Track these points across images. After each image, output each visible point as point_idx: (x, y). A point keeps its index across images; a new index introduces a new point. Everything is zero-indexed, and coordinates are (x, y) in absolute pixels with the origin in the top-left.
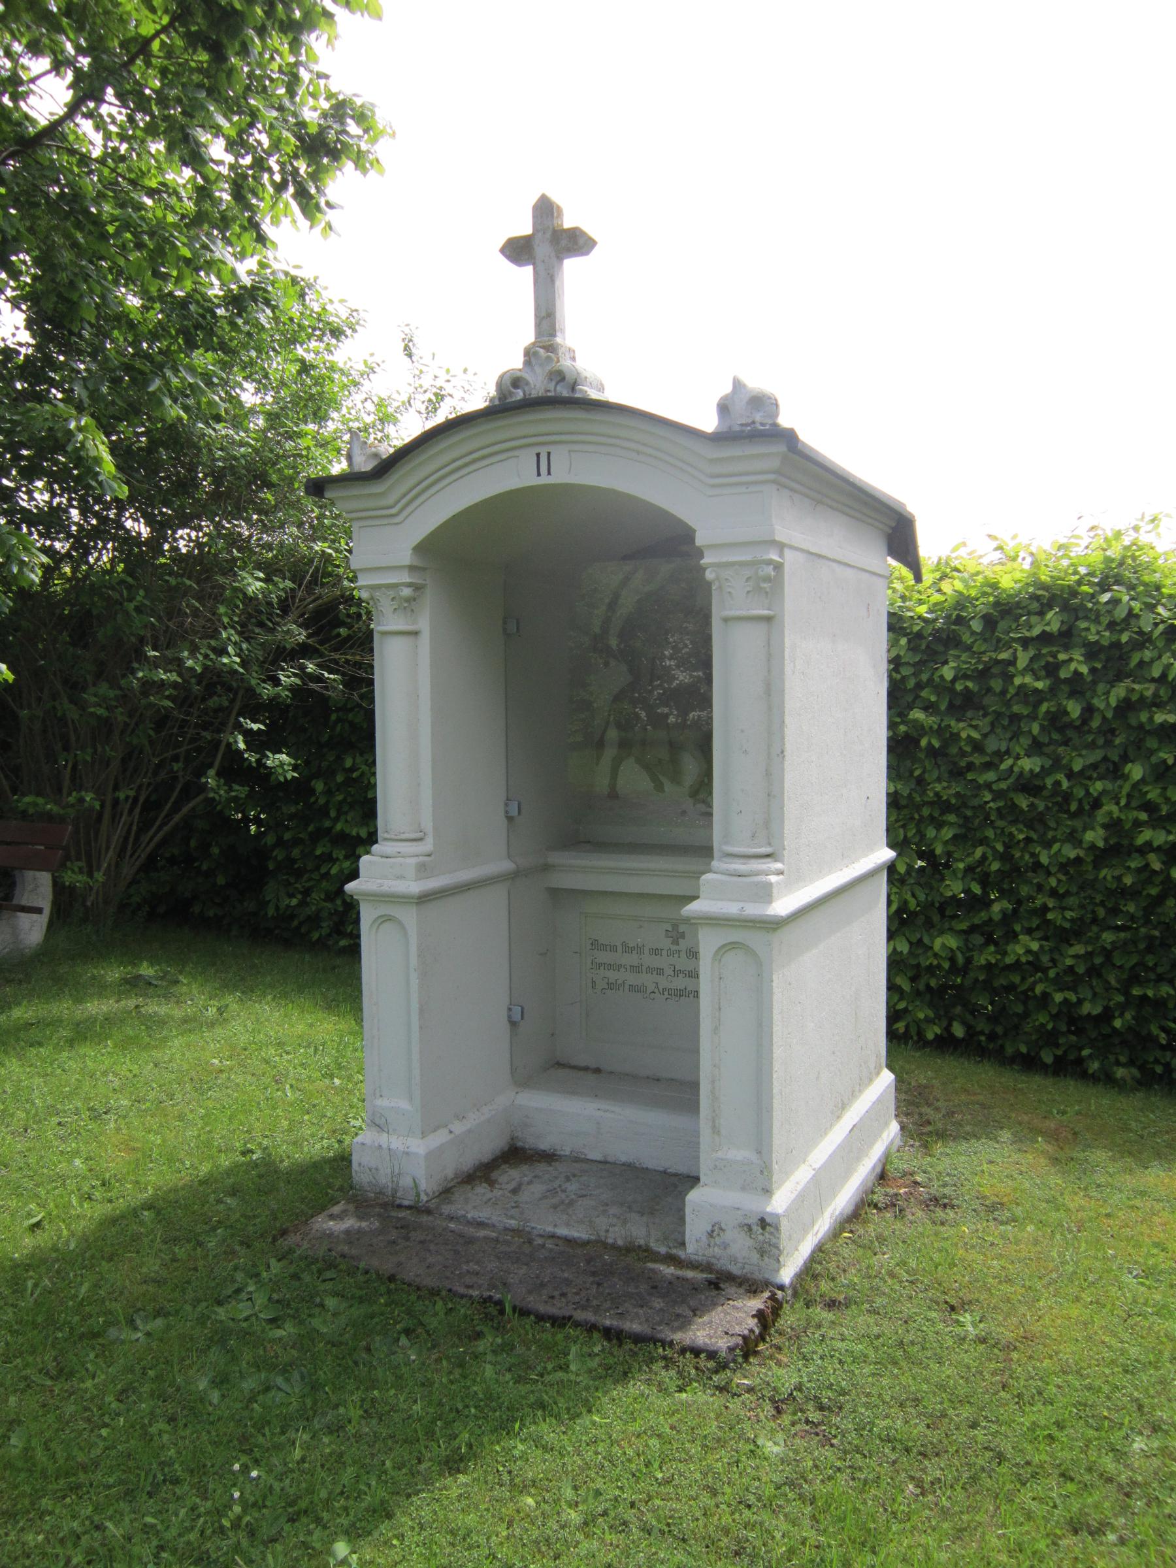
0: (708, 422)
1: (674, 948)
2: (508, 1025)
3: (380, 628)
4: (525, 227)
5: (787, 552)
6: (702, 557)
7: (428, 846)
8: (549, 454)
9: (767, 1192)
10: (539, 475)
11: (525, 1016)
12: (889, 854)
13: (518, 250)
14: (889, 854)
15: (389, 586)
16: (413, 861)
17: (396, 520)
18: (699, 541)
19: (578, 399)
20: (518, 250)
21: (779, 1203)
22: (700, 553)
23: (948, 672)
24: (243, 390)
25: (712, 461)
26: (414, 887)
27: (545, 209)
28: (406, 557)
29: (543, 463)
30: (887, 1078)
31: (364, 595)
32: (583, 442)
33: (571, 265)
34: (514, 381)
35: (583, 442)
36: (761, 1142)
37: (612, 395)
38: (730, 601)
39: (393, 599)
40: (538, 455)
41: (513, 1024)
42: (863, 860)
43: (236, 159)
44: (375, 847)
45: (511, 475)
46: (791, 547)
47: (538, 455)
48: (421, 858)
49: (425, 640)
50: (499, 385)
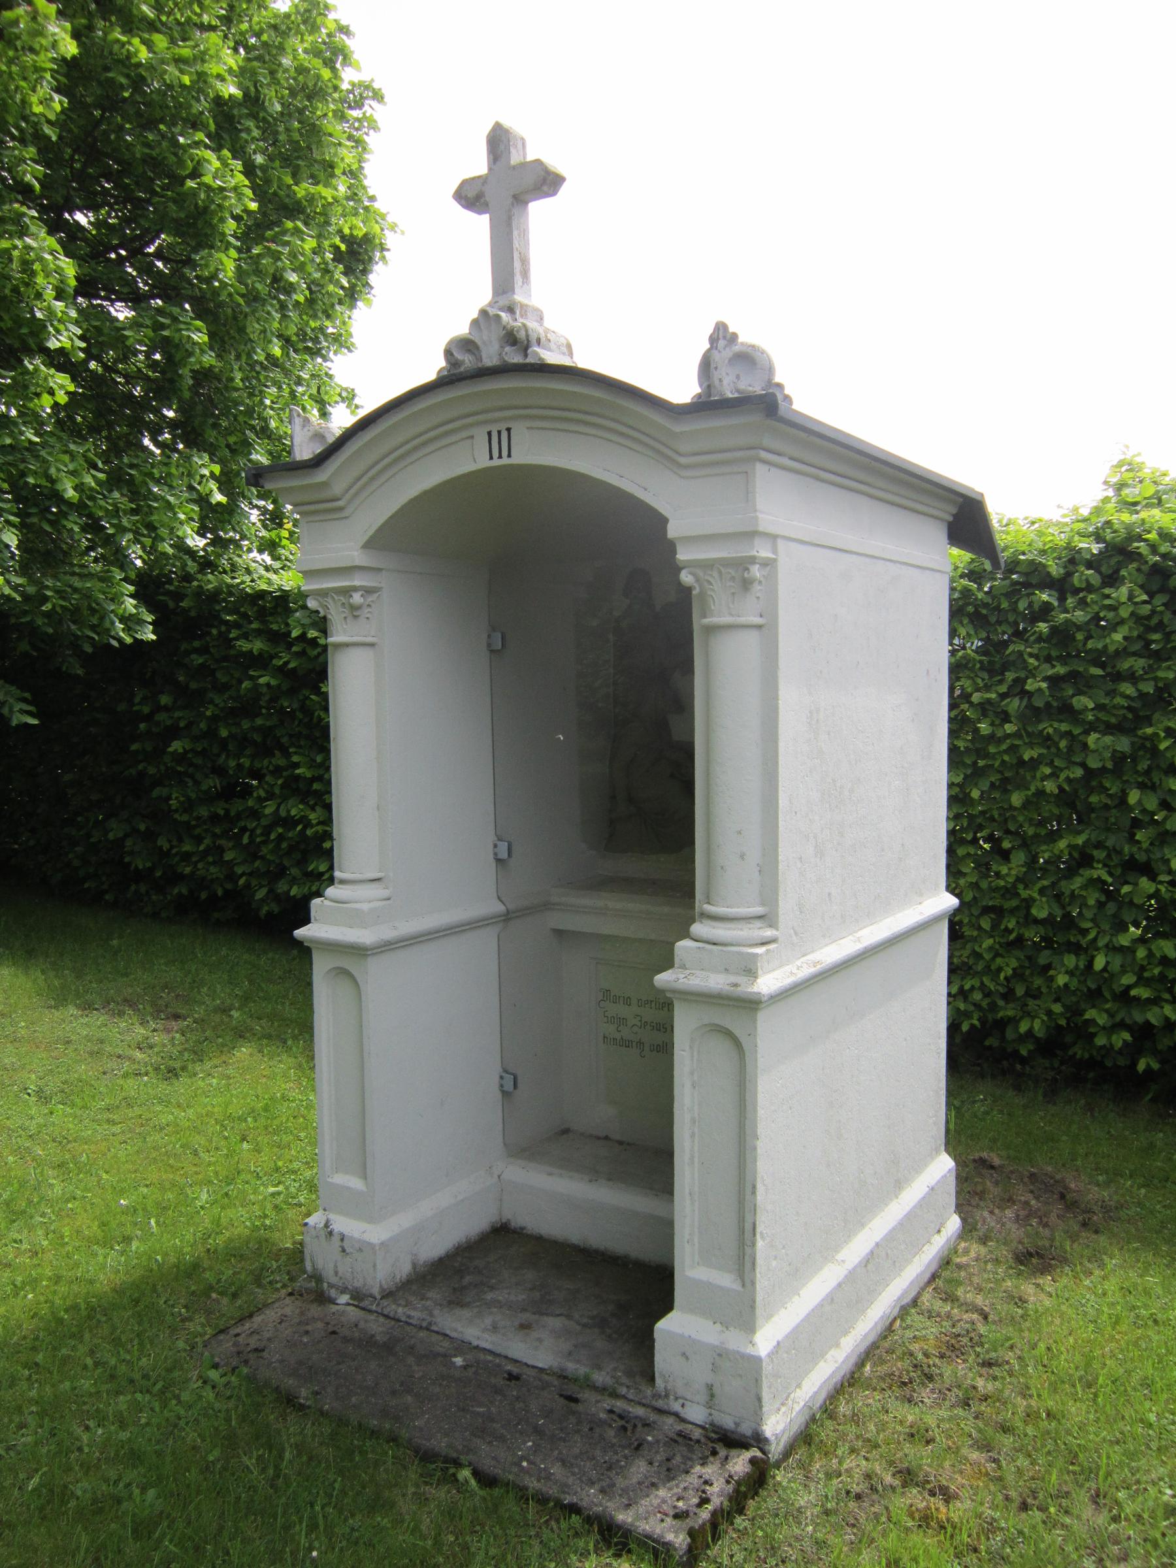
0: (679, 386)
2: (499, 1095)
4: (480, 166)
5: (781, 544)
9: (750, 1327)
10: (491, 458)
11: (519, 1085)
12: (952, 902)
13: (471, 196)
14: (952, 902)
18: (672, 532)
19: (532, 365)
20: (471, 196)
21: (764, 1341)
23: (262, 681)
27: (499, 141)
29: (500, 440)
30: (945, 1164)
32: (622, 434)
33: (538, 210)
34: (466, 344)
35: (622, 434)
36: (742, 1261)
37: (583, 360)
38: (718, 608)
40: (489, 434)
41: (505, 1094)
44: (330, 891)
45: (470, 458)
46: (784, 538)
47: (489, 434)
50: (448, 353)
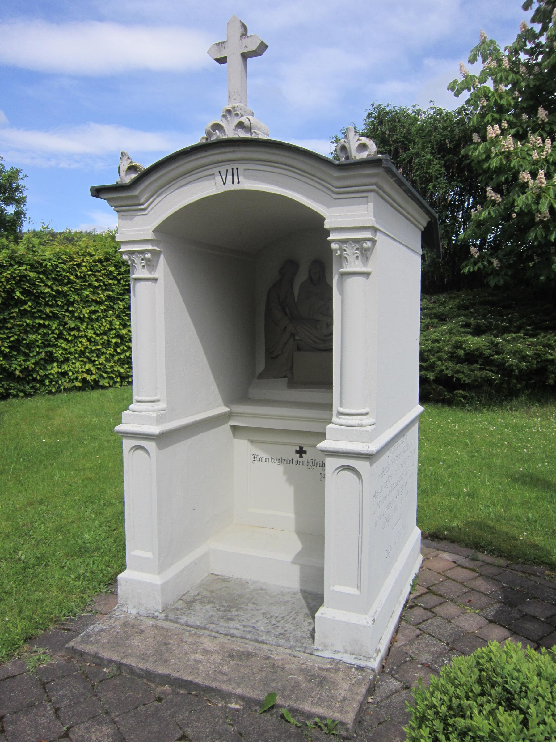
1: (300, 459)
3: (133, 276)
6: (329, 236)
7: (162, 405)
8: (237, 169)
10: (233, 183)
15: (142, 252)
16: (154, 415)
17: (146, 212)
18: (326, 226)
22: (327, 232)
24: (204, 643)
25: (338, 179)
26: (155, 430)
28: (150, 235)
31: (125, 257)
39: (142, 260)
42: (334, 280)
43: (145, 257)
47: (233, 169)
48: (158, 413)
49: (161, 281)
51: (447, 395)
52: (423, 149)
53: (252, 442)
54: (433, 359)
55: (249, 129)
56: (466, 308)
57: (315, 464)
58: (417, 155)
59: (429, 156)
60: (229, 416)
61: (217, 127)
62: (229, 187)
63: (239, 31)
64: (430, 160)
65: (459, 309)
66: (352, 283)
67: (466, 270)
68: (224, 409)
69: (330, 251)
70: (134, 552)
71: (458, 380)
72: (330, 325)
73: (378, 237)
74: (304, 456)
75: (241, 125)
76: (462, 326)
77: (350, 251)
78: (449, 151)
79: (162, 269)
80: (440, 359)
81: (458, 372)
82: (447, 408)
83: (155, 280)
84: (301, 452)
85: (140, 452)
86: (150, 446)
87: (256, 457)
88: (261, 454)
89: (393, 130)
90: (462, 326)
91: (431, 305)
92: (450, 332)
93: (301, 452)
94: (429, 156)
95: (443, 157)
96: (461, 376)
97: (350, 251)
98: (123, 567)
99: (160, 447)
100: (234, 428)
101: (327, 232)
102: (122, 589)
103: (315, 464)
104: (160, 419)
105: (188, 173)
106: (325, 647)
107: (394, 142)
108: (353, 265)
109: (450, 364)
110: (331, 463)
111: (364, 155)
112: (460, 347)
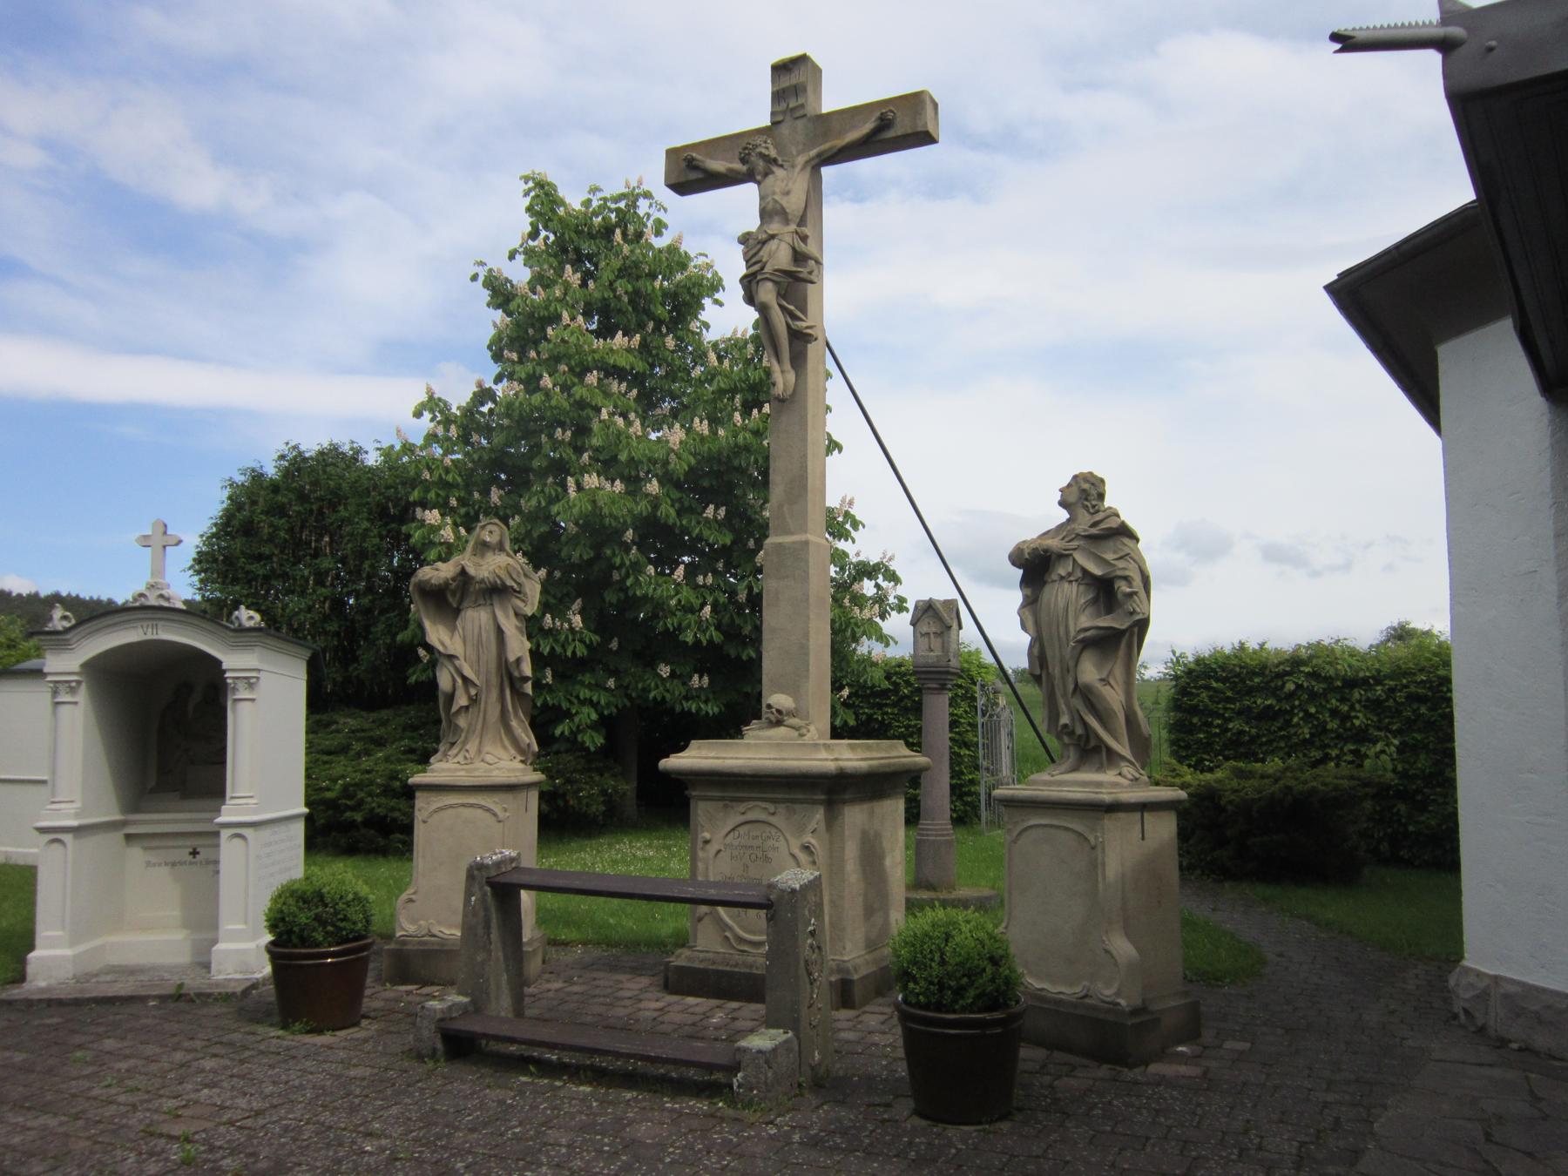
18: (224, 666)
22: (225, 671)
51: (381, 841)
52: (358, 513)
53: (145, 849)
54: (361, 795)
55: (168, 599)
56: (414, 728)
57: (208, 862)
58: (349, 521)
59: (366, 524)
60: (124, 824)
61: (142, 595)
62: (150, 636)
63: (162, 529)
64: (366, 530)
65: (404, 729)
66: (241, 705)
67: (413, 679)
68: (118, 817)
69: (226, 685)
70: (43, 932)
71: (394, 820)
72: (225, 734)
73: (261, 675)
74: (200, 849)
75: (162, 596)
76: (405, 752)
77: (241, 685)
78: (393, 518)
79: (82, 696)
80: (370, 794)
81: (393, 809)
82: (381, 859)
83: (75, 703)
84: (194, 853)
85: (56, 846)
86: (67, 838)
87: (148, 864)
88: (153, 860)
89: (315, 483)
90: (405, 752)
91: (367, 726)
92: (387, 759)
93: (194, 853)
94: (366, 524)
95: (387, 524)
96: (396, 814)
97: (241, 685)
98: (32, 948)
99: (75, 837)
100: (128, 837)
101: (225, 671)
102: (30, 969)
103: (208, 862)
104: (77, 816)
105: (115, 624)
106: (220, 972)
107: (318, 499)
108: (243, 694)
109: (383, 800)
110: (225, 834)
111: (251, 624)
112: (396, 778)
